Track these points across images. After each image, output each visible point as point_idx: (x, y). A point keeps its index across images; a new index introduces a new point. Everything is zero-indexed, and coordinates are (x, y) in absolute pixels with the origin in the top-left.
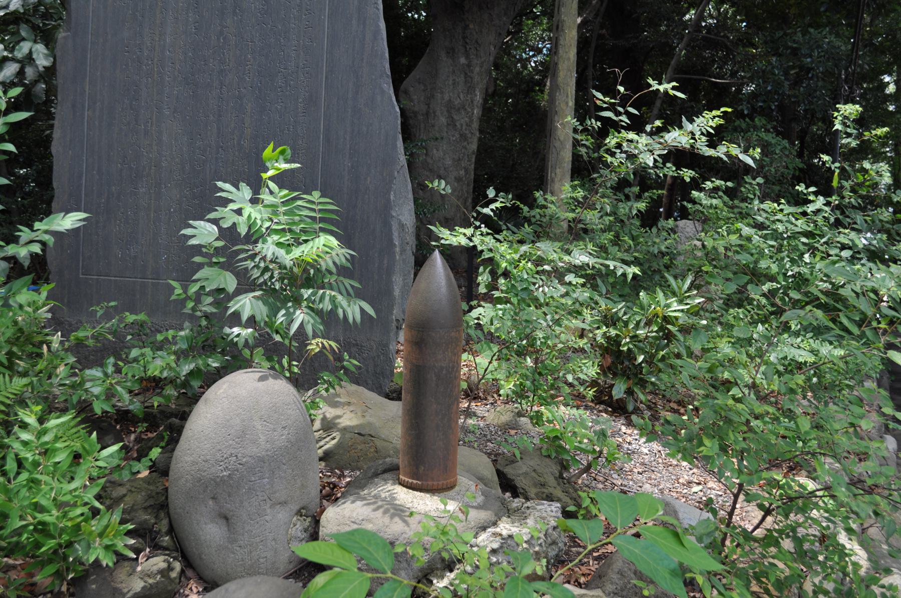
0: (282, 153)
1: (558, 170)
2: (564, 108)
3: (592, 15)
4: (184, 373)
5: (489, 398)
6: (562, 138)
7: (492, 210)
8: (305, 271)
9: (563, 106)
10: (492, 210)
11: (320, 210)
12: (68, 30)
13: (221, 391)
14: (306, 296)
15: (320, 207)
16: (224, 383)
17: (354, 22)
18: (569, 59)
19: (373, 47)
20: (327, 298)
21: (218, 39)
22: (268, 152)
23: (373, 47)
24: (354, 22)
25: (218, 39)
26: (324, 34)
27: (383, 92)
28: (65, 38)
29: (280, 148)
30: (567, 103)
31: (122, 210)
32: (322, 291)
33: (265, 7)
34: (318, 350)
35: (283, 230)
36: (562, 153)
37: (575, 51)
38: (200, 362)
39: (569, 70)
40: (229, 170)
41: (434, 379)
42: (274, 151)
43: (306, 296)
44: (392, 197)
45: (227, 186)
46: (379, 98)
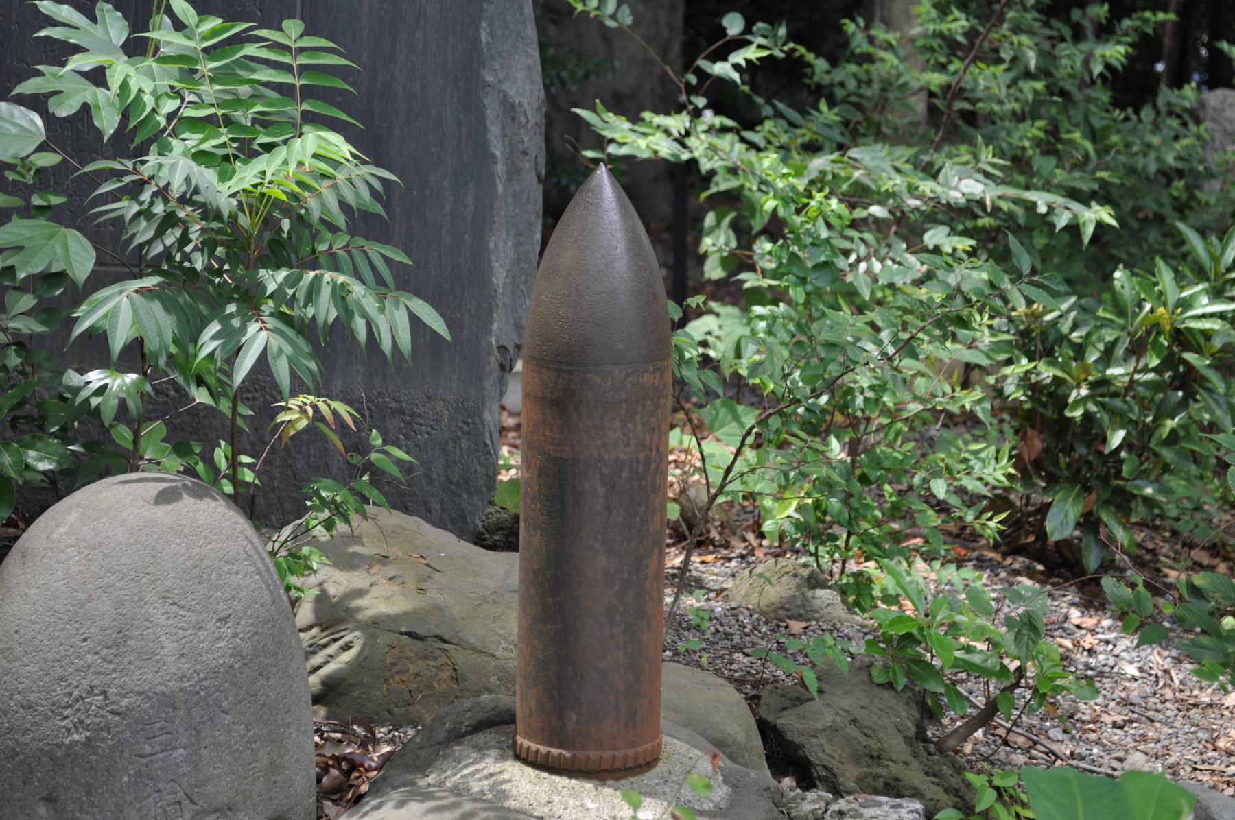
7: (736, 67)
8: (269, 223)
10: (736, 67)
11: (303, 69)
13: (63, 530)
14: (271, 288)
15: (303, 60)
16: (69, 510)
32: (312, 274)
34: (303, 424)
41: (601, 491)
44: (484, 37)
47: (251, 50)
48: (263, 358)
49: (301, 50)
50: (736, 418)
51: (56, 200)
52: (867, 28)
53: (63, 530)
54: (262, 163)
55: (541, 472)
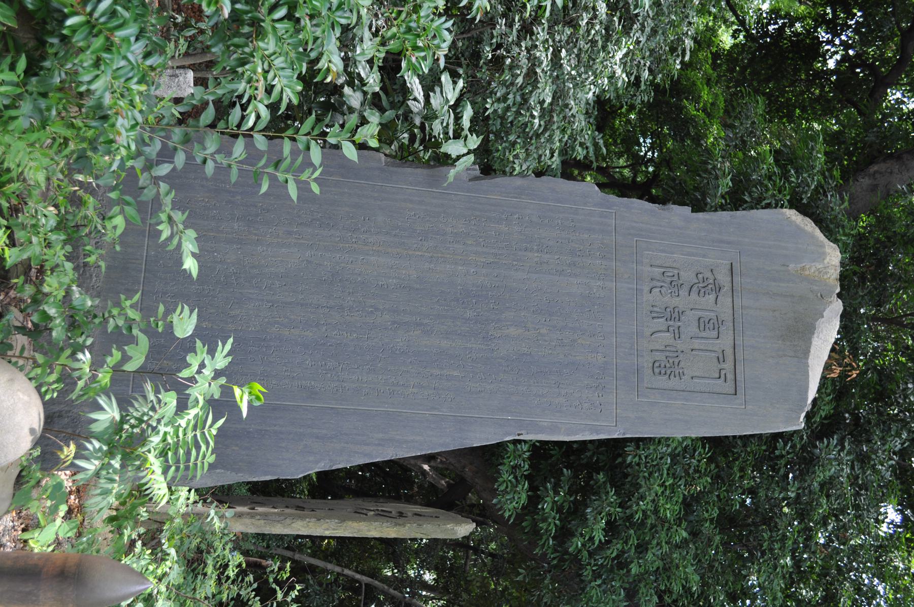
0: (258, 398)
1: (263, 522)
2: (323, 527)
3: (431, 480)
4: (46, 309)
5: (20, 521)
6: (293, 525)
7: (213, 518)
8: (138, 457)
9: (325, 526)
10: (213, 518)
11: (196, 464)
12: (387, 164)
13: (21, 396)
14: (113, 462)
15: (199, 464)
16: (29, 396)
17: (380, 436)
18: (369, 531)
19: (357, 453)
20: (110, 486)
21: (371, 306)
22: (258, 387)
23: (357, 453)
24: (380, 436)
25: (371, 306)
26: (373, 407)
27: (317, 462)
28: (380, 160)
29: (261, 396)
30: (328, 529)
31: (218, 205)
32: (117, 478)
33: (398, 352)
34: (62, 457)
35: (178, 437)
36: (279, 525)
37: (377, 536)
38: (58, 321)
39: (359, 531)
40: (251, 312)
41: (28, 590)
42: (260, 391)
43: (113, 462)
44: (218, 471)
45: (228, 347)
46: (311, 458)
47: (203, 448)
48: (85, 470)
49: (203, 463)
50: (71, 530)
51: (162, 309)
52: (231, 541)
53: (21, 396)
54: (159, 471)
55: (36, 565)
